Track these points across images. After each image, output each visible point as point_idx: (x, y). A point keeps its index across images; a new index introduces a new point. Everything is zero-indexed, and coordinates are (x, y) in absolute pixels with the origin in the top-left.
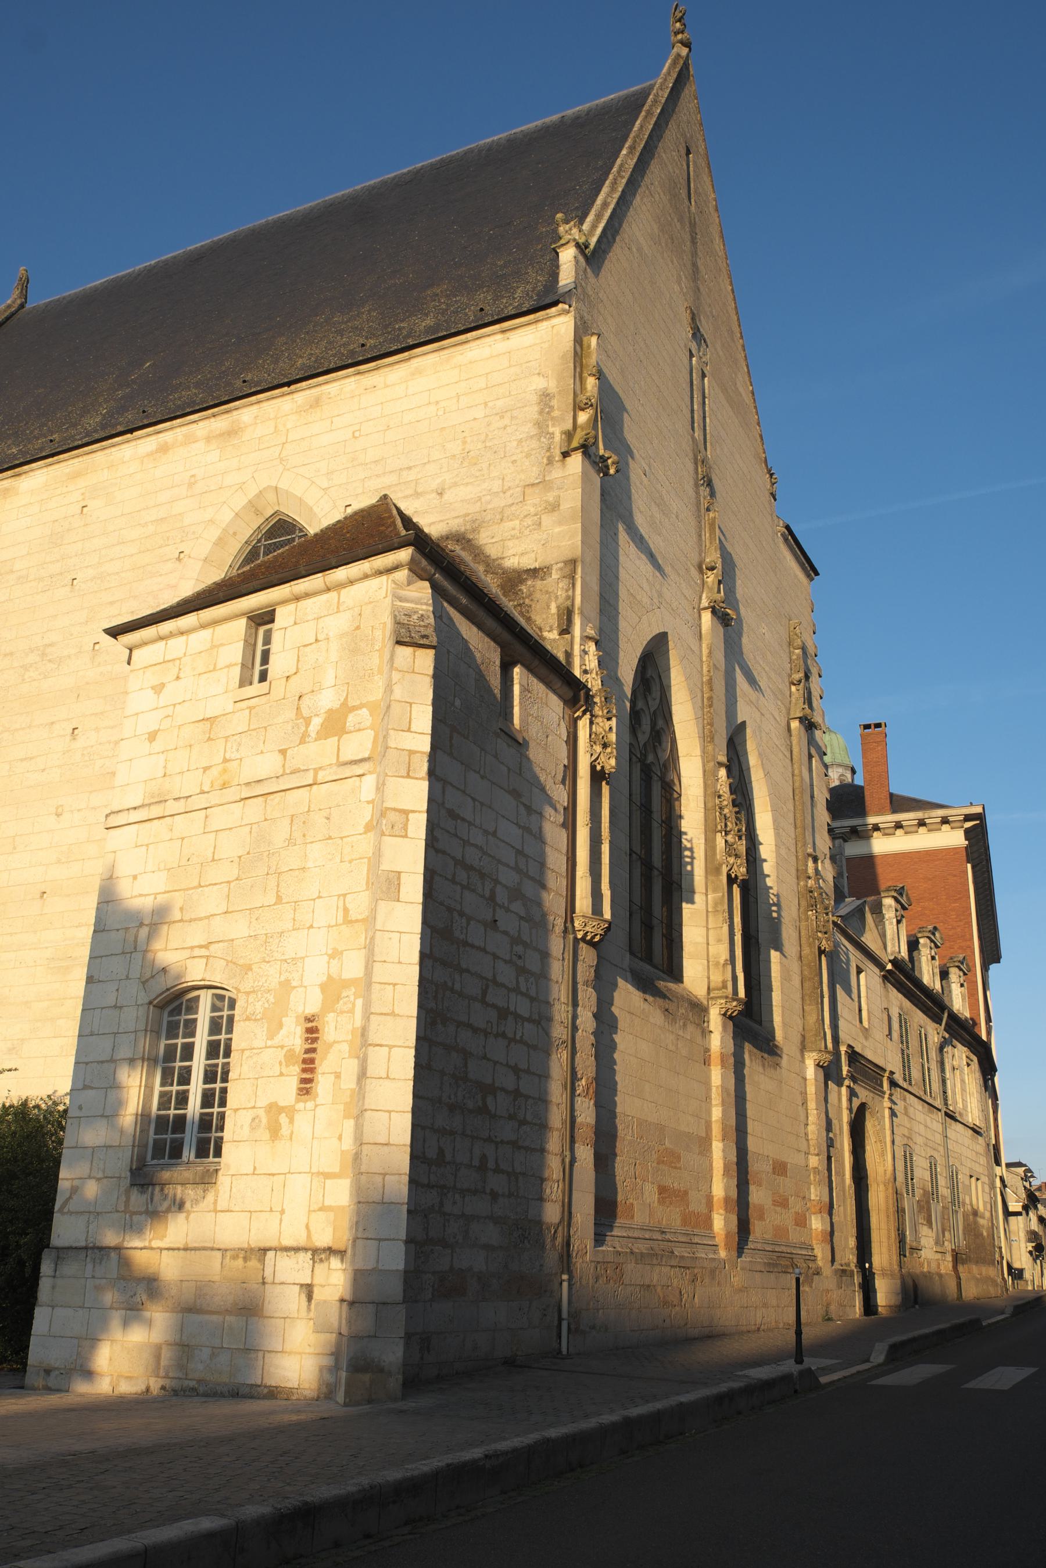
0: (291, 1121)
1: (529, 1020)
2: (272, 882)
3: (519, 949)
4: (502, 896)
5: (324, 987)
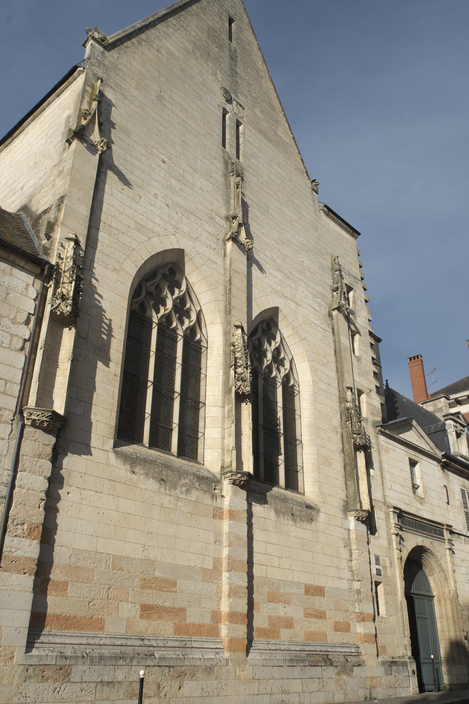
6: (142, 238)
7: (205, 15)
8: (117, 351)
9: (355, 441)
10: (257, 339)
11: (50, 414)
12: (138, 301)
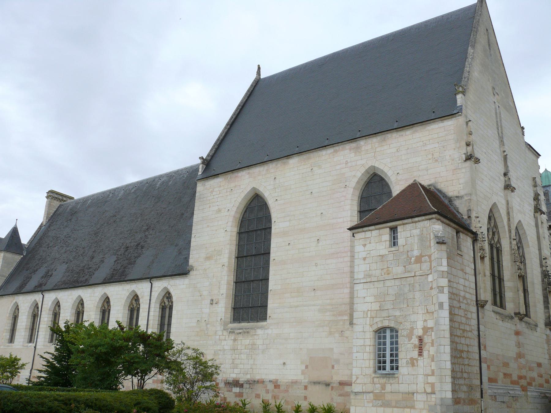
0: (417, 362)
1: (470, 331)
2: (405, 301)
3: (466, 313)
4: (461, 300)
5: (423, 329)
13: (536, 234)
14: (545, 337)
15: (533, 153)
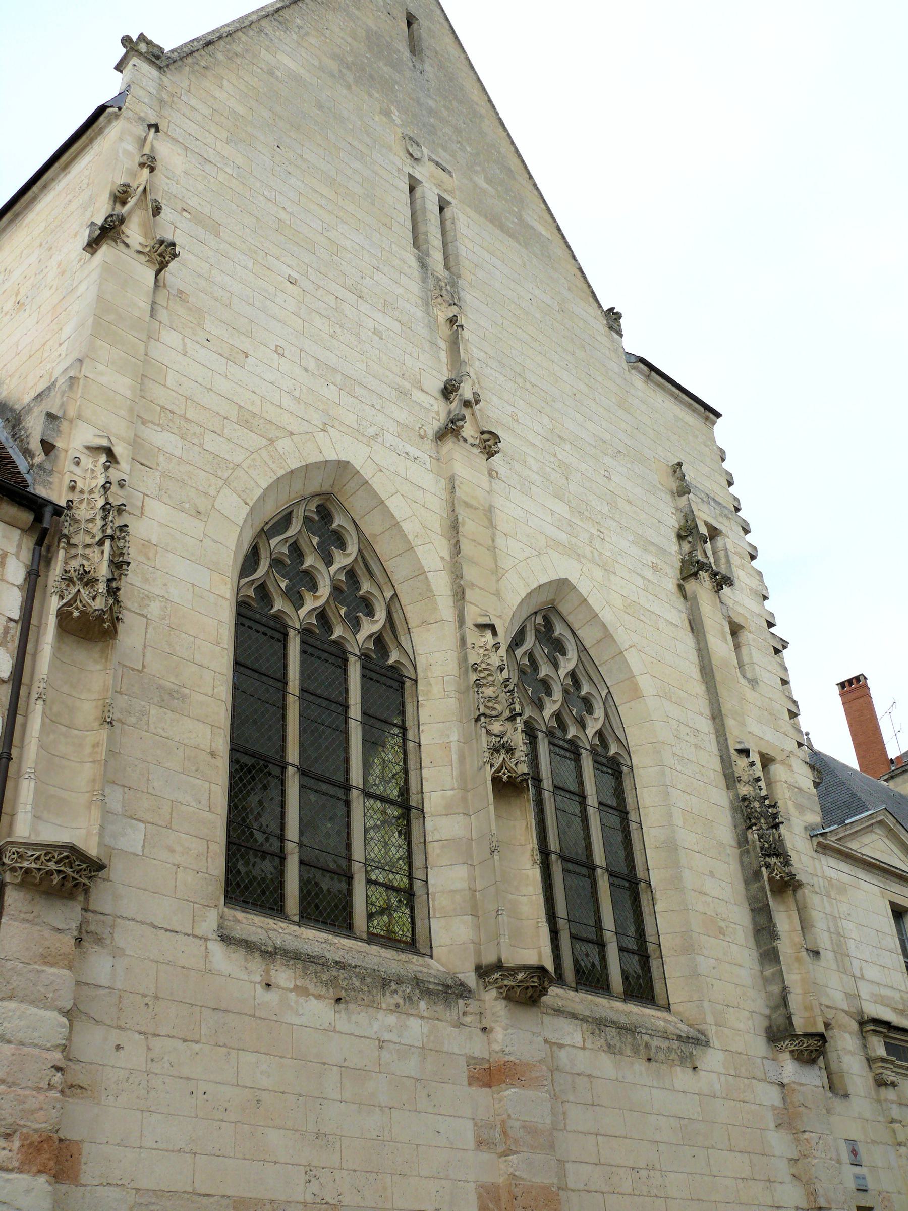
6: (254, 440)
7: (358, 9)
8: (212, 696)
9: (771, 873)
10: (525, 653)
11: (65, 854)
12: (253, 581)
13: (693, 656)
14: (773, 1096)
15: (689, 406)
